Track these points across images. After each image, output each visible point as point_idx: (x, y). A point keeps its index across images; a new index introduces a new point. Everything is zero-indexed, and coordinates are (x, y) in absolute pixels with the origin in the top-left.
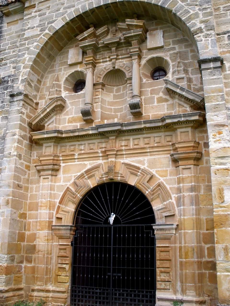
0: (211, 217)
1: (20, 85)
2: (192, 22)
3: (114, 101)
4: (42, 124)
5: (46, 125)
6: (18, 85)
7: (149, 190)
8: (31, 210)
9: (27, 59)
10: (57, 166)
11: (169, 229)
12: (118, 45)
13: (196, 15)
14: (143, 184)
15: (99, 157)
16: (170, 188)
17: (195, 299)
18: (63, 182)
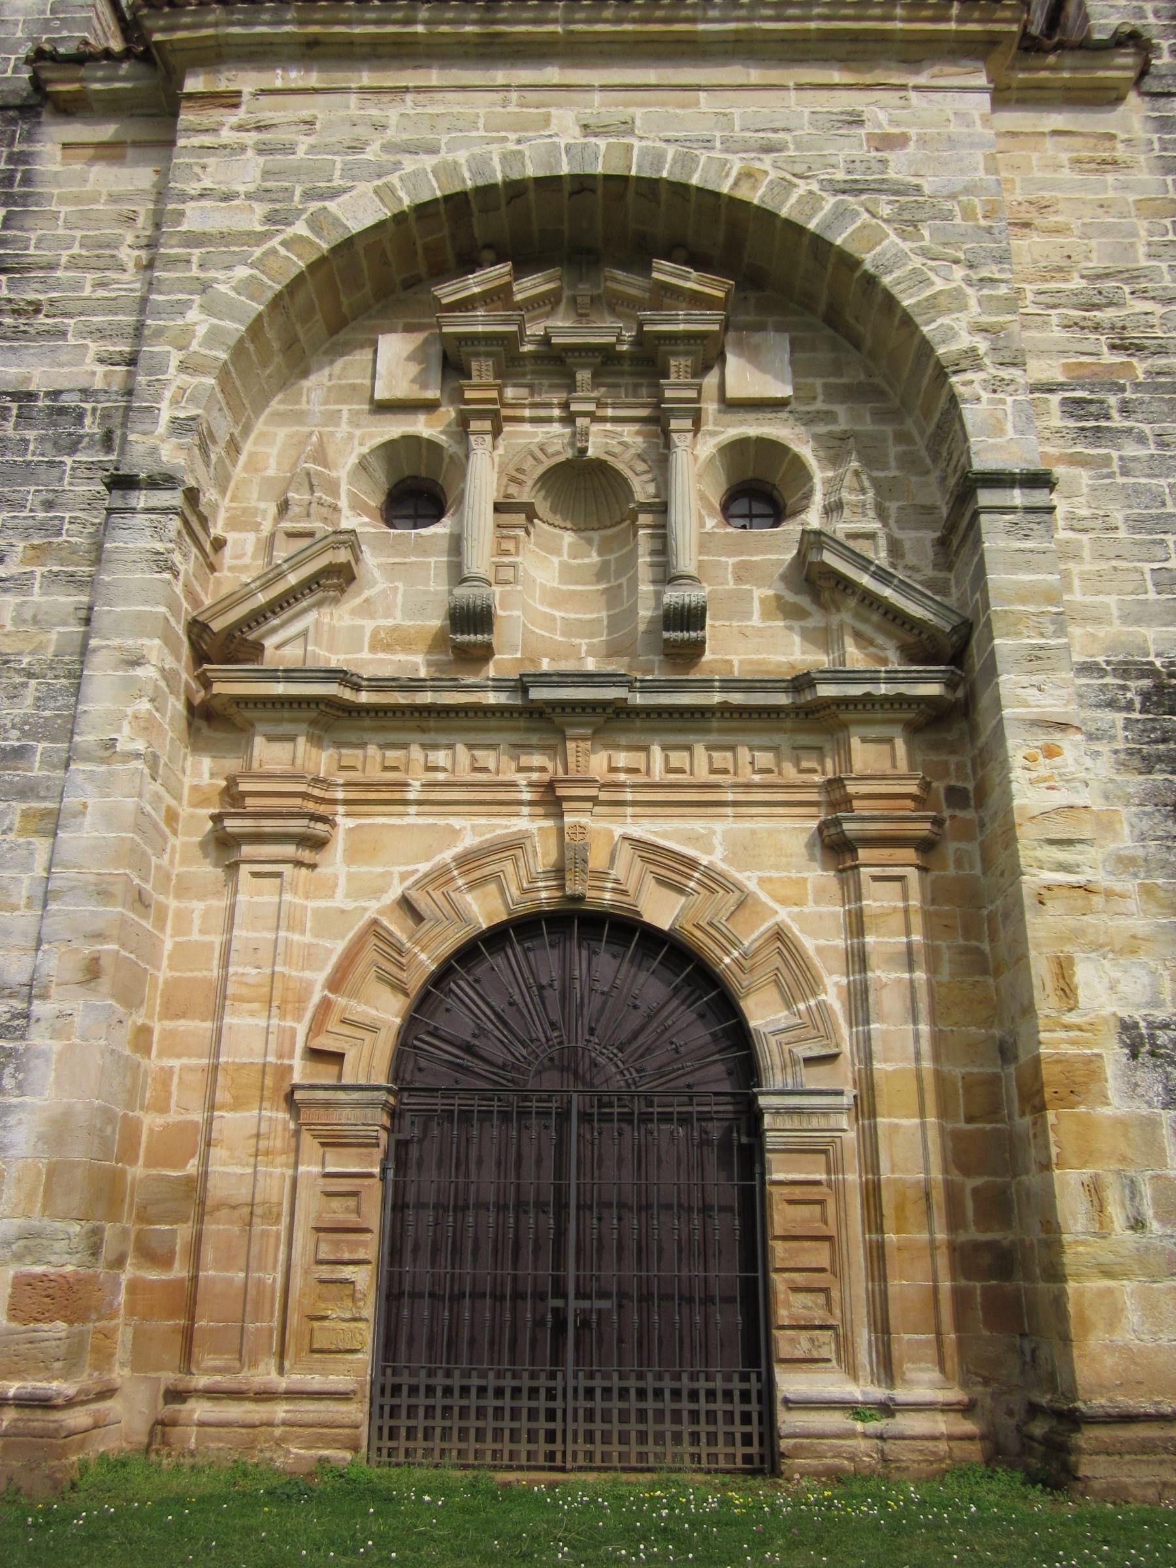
0: (981, 1070)
1: (163, 441)
2: (939, 321)
3: (564, 587)
4: (251, 637)
5: (269, 643)
6: (151, 441)
7: (736, 954)
8: (177, 1016)
9: (201, 331)
10: (326, 827)
11: (826, 1111)
12: (605, 361)
13: (957, 300)
14: (711, 924)
15: (520, 803)
16: (819, 950)
17: (940, 1396)
18: (348, 895)
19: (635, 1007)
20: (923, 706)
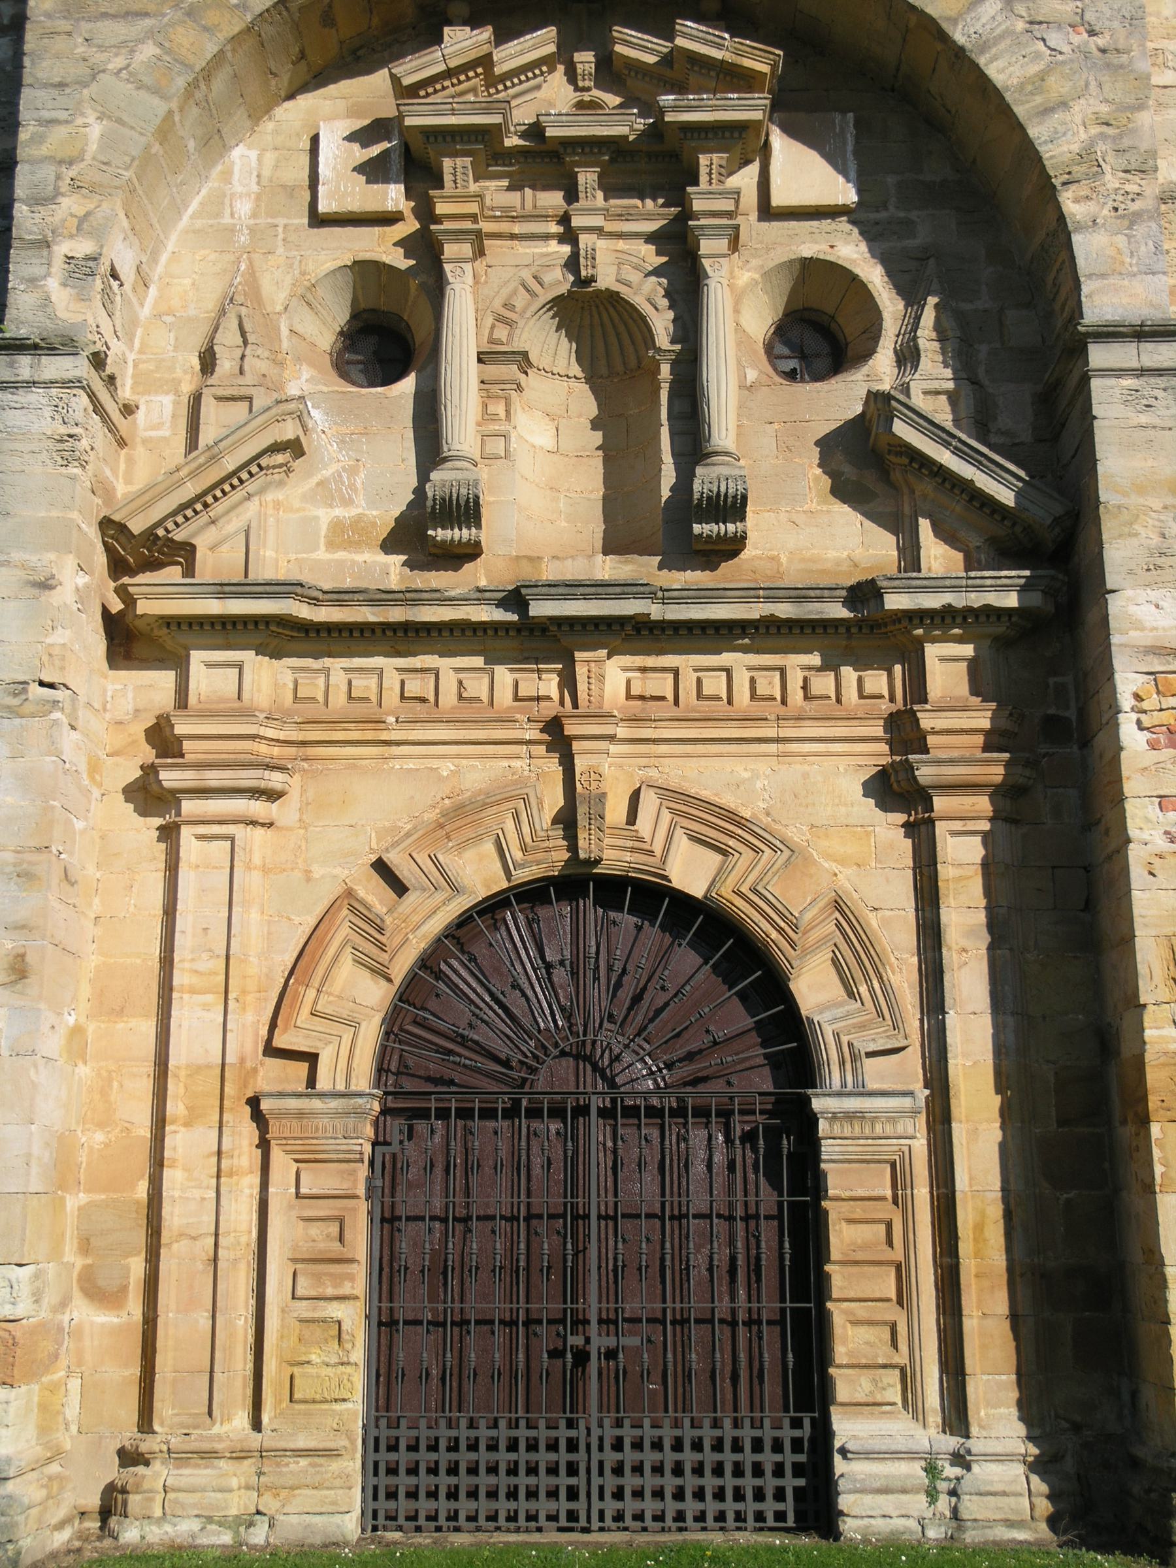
14: (754, 890)
19: (663, 988)
20: (1014, 619)
